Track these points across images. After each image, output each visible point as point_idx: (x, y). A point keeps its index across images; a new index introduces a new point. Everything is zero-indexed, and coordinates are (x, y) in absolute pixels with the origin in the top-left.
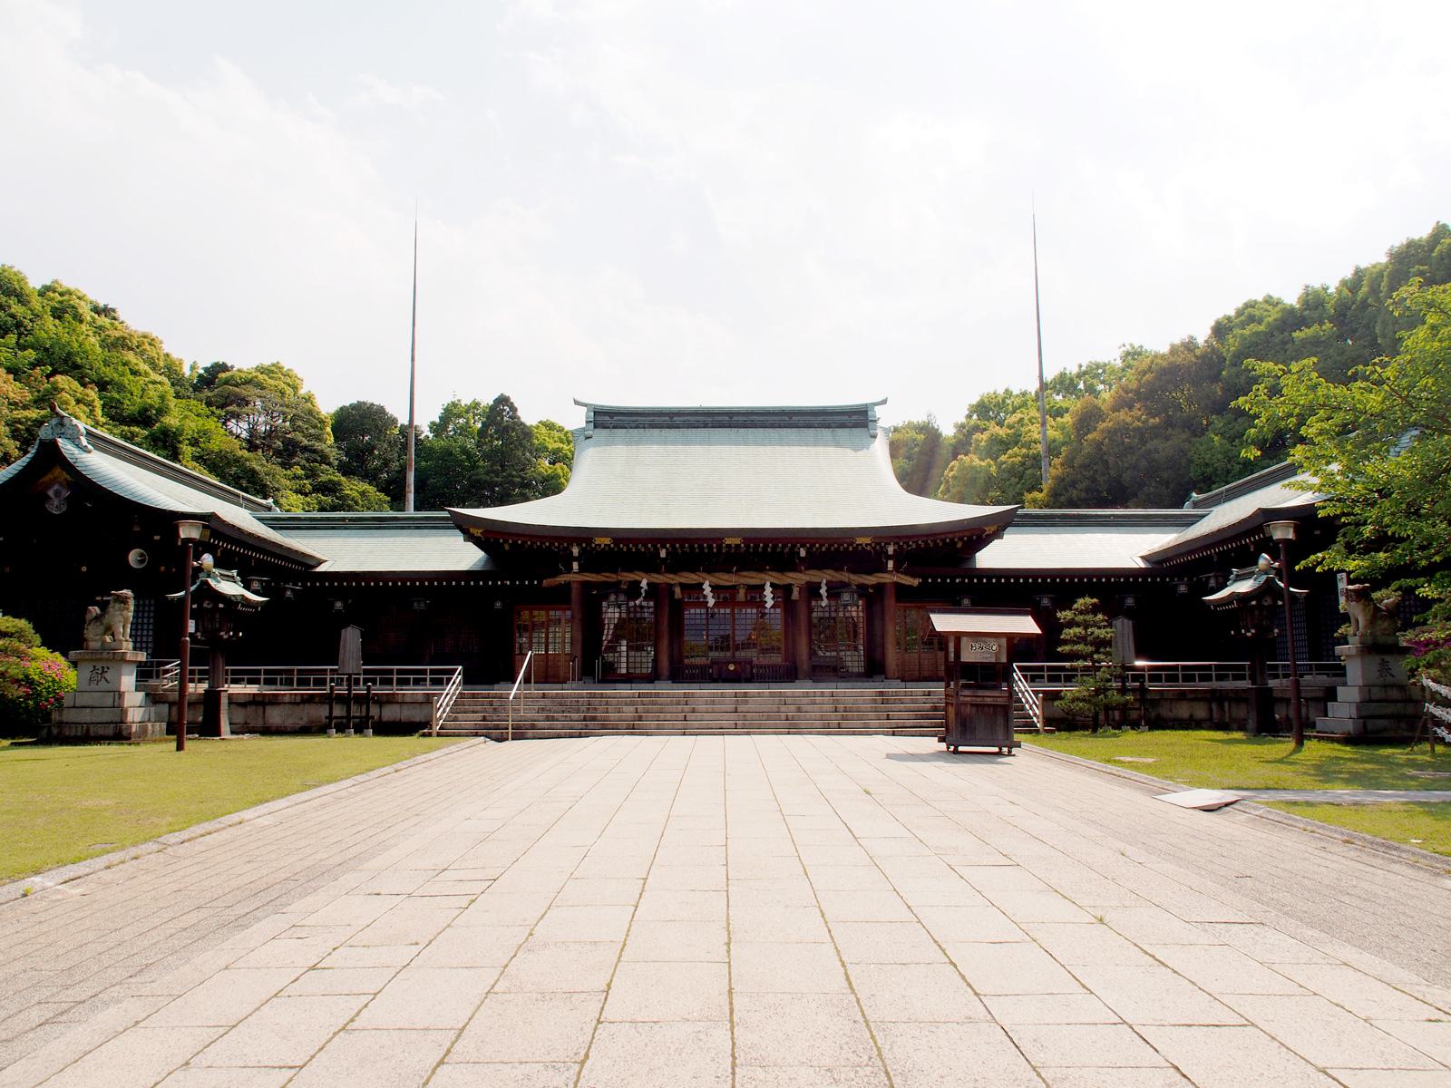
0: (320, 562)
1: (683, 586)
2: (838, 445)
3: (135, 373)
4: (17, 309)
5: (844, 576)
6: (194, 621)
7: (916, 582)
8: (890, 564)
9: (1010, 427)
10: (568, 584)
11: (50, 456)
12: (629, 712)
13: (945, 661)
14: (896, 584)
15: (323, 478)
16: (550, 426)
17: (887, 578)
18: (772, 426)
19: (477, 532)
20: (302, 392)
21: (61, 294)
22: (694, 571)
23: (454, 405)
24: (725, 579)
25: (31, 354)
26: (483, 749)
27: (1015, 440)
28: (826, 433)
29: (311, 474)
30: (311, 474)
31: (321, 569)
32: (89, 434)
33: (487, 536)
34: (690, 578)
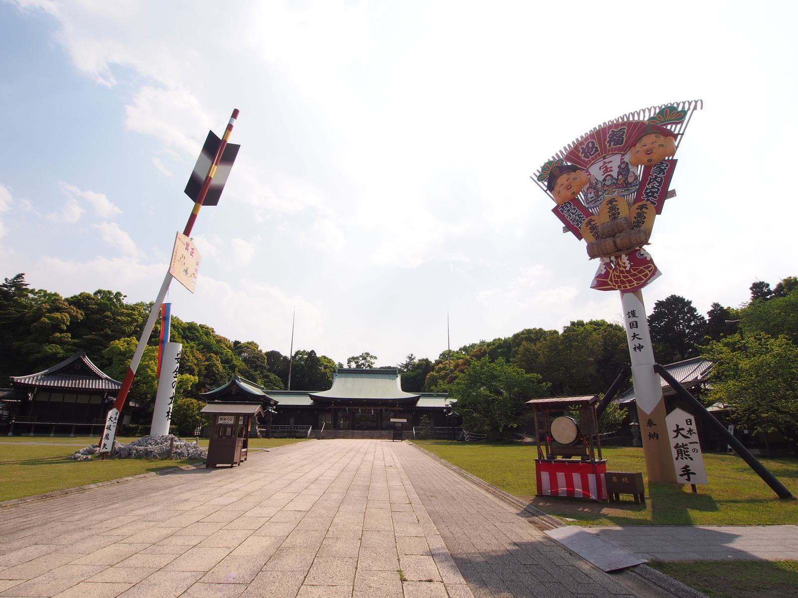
0: (278, 402)
1: (355, 409)
2: (389, 379)
3: (224, 349)
4: (197, 334)
5: (388, 408)
6: (597, 449)
7: (403, 409)
8: (397, 406)
9: (444, 365)
10: (331, 409)
11: (234, 383)
12: (342, 435)
13: (393, 426)
14: (399, 410)
15: (265, 374)
16: (325, 357)
17: (397, 409)
18: (376, 374)
19: (313, 398)
20: (259, 349)
21: (206, 329)
22: (357, 406)
23: (298, 351)
24: (363, 408)
25: (202, 346)
26: (315, 441)
27: (444, 368)
28: (387, 375)
29: (262, 373)
30: (262, 373)
31: (279, 404)
32: (241, 379)
33: (312, 397)
34: (357, 408)
